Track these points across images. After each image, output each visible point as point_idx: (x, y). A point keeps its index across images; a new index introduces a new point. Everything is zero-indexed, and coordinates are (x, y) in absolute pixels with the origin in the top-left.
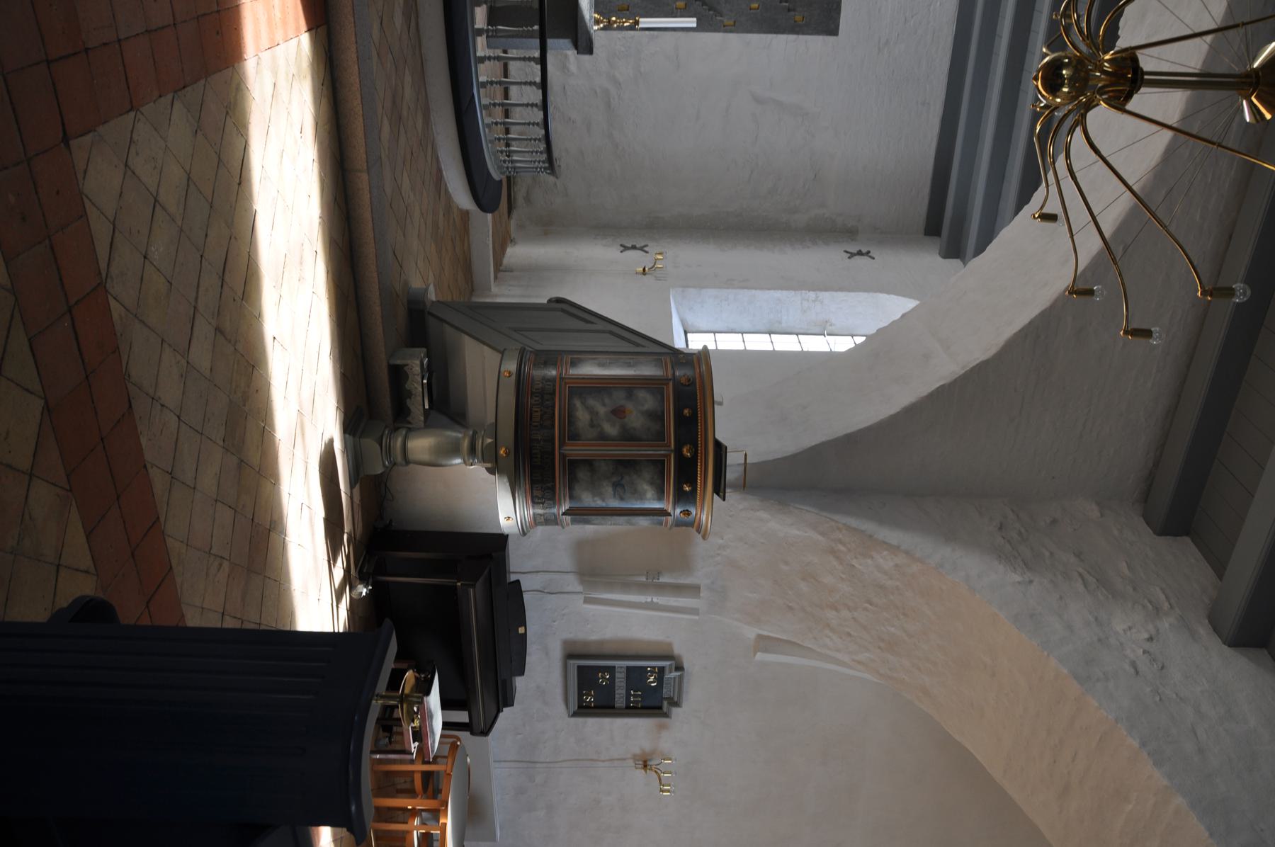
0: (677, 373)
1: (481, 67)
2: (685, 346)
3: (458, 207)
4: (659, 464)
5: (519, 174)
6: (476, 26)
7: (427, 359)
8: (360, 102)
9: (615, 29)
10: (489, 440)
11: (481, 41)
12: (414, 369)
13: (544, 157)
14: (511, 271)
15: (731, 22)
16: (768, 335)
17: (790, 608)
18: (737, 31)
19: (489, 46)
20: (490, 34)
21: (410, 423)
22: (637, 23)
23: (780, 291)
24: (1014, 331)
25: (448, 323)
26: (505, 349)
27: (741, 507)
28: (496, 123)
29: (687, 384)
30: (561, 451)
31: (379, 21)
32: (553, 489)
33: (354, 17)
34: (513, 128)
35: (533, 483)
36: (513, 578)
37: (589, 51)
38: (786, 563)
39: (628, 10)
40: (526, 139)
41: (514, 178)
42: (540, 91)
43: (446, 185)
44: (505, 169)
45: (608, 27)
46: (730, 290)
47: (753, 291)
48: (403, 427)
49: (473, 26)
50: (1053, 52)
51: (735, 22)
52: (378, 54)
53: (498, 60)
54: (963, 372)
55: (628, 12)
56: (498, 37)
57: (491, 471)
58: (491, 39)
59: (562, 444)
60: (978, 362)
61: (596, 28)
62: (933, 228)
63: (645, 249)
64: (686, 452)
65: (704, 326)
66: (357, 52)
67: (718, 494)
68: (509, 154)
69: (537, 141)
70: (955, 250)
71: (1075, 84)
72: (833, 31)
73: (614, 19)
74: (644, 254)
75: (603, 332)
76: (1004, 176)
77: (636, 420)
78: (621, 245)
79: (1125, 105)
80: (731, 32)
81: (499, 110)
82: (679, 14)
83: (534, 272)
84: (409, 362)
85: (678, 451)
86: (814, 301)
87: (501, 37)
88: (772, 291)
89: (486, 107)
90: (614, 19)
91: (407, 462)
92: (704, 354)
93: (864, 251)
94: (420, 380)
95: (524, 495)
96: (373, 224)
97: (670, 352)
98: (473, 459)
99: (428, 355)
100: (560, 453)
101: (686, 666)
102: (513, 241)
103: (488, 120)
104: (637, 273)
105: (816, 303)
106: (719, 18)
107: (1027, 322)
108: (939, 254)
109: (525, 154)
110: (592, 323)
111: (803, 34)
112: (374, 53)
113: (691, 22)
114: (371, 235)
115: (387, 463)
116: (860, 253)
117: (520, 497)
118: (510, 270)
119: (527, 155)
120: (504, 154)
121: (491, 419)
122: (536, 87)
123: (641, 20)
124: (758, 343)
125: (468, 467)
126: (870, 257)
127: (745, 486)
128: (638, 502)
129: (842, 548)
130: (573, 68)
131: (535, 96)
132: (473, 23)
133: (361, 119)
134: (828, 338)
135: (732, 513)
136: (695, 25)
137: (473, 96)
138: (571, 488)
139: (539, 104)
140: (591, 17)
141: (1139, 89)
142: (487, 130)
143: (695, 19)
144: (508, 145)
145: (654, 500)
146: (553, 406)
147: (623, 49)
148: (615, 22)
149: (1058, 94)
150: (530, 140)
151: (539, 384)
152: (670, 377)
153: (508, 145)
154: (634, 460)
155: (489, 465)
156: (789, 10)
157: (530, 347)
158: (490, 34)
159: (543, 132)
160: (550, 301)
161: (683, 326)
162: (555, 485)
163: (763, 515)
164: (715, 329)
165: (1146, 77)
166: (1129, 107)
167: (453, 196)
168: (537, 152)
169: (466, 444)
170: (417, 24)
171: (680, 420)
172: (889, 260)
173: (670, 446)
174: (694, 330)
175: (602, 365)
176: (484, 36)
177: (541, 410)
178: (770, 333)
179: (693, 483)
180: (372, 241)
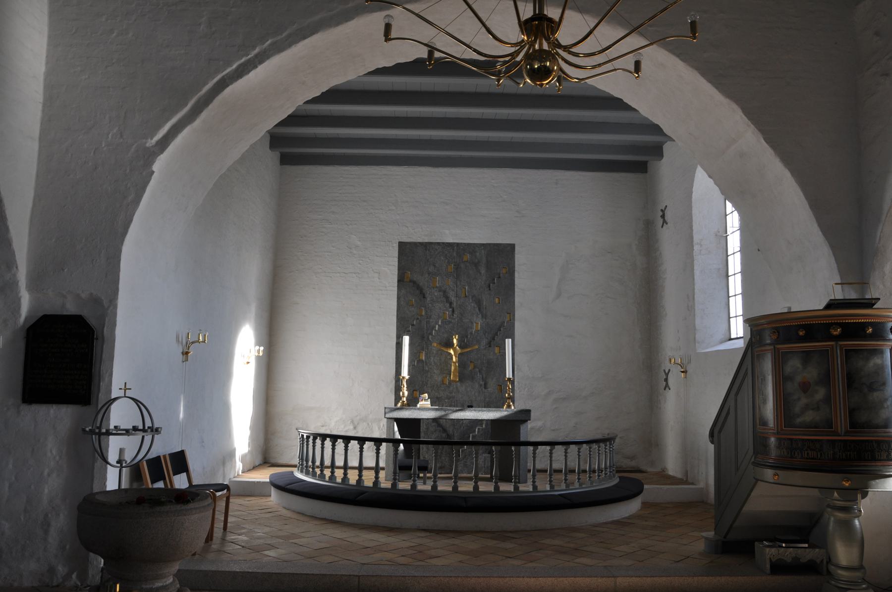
0: (768, 342)
1: (540, 488)
2: (742, 339)
3: (640, 510)
5: (615, 464)
6: (513, 490)
7: (764, 542)
8: (565, 579)
9: (514, 394)
10: (836, 494)
11: (522, 487)
12: (774, 554)
13: (602, 445)
14: (687, 472)
15: (508, 315)
16: (730, 278)
19: (525, 482)
20: (517, 481)
21: (822, 561)
22: (509, 379)
23: (695, 271)
24: (717, 92)
25: (734, 522)
26: (754, 478)
27: (881, 286)
28: (579, 479)
29: (777, 334)
30: (843, 434)
31: (509, 559)
32: (879, 443)
33: (506, 577)
34: (582, 468)
35: (874, 459)
37: (527, 412)
39: (501, 386)
40: (590, 458)
41: (617, 468)
42: (556, 446)
43: (624, 518)
44: (611, 474)
45: (512, 399)
46: (696, 308)
47: (696, 291)
48: (827, 569)
49: (512, 492)
50: (523, 77)
51: (508, 313)
52: (531, 562)
53: (535, 476)
54: (752, 125)
55: (502, 386)
56: (519, 475)
57: (865, 495)
58: (521, 481)
59: (836, 433)
60: (744, 116)
61: (513, 407)
62: (640, 167)
63: (667, 371)
64: (837, 332)
65: (725, 326)
66: (530, 577)
67: (874, 304)
68: (600, 470)
69: (591, 450)
70: (657, 151)
71: (544, 58)
72: (512, 246)
73: (507, 395)
74: (670, 372)
75: (736, 401)
76: (603, 123)
77: (811, 373)
78: (665, 389)
79: (557, 22)
80: (514, 315)
81: (569, 477)
82: (503, 351)
83: (688, 453)
84: (768, 557)
86: (701, 245)
87: (519, 473)
88: (695, 277)
89: (567, 486)
90: (507, 395)
91: (860, 568)
92: (751, 322)
93: (661, 213)
94: (783, 549)
95: (887, 467)
96: (656, 576)
97: (750, 348)
98: (854, 509)
99: (761, 541)
100: (844, 436)
102: (664, 470)
103: (577, 485)
104: (686, 377)
105: (702, 244)
106: (505, 324)
107: (710, 84)
108: (660, 160)
109: (600, 459)
110: (729, 410)
111: (514, 267)
112: (531, 565)
113: (508, 342)
114: (664, 579)
115: (864, 586)
116: (663, 216)
117: (888, 470)
118: (686, 473)
119: (601, 457)
120: (600, 474)
121: (816, 492)
122: (553, 449)
123: (507, 377)
124: (736, 284)
125: (863, 514)
126: (665, 209)
127: (863, 283)
128: (886, 370)
130: (539, 424)
131: (559, 450)
132: (510, 492)
133: (578, 579)
134: (728, 233)
135: (888, 294)
136: (510, 340)
137: (559, 495)
138: (878, 427)
139: (565, 448)
140: (506, 411)
141: (546, 15)
142: (583, 486)
143: (506, 340)
144: (594, 471)
145: (883, 357)
146: (803, 440)
147: (526, 389)
148: (509, 394)
149: (551, 69)
150: (590, 455)
151: (783, 452)
152: (772, 347)
153: (594, 471)
154: (847, 375)
155: (859, 496)
157: (752, 457)
158: (517, 481)
159: (584, 445)
160: (712, 442)
161: (725, 341)
162: (875, 440)
164: (727, 317)
165: (537, 13)
166: (557, 19)
167: (631, 514)
168: (599, 450)
169: (841, 515)
170: (511, 532)
171: (809, 338)
172: (667, 196)
173: (832, 345)
174: (728, 333)
175: (765, 401)
176: (519, 485)
177: (807, 450)
178: (727, 276)
179: (864, 326)
180: (669, 578)
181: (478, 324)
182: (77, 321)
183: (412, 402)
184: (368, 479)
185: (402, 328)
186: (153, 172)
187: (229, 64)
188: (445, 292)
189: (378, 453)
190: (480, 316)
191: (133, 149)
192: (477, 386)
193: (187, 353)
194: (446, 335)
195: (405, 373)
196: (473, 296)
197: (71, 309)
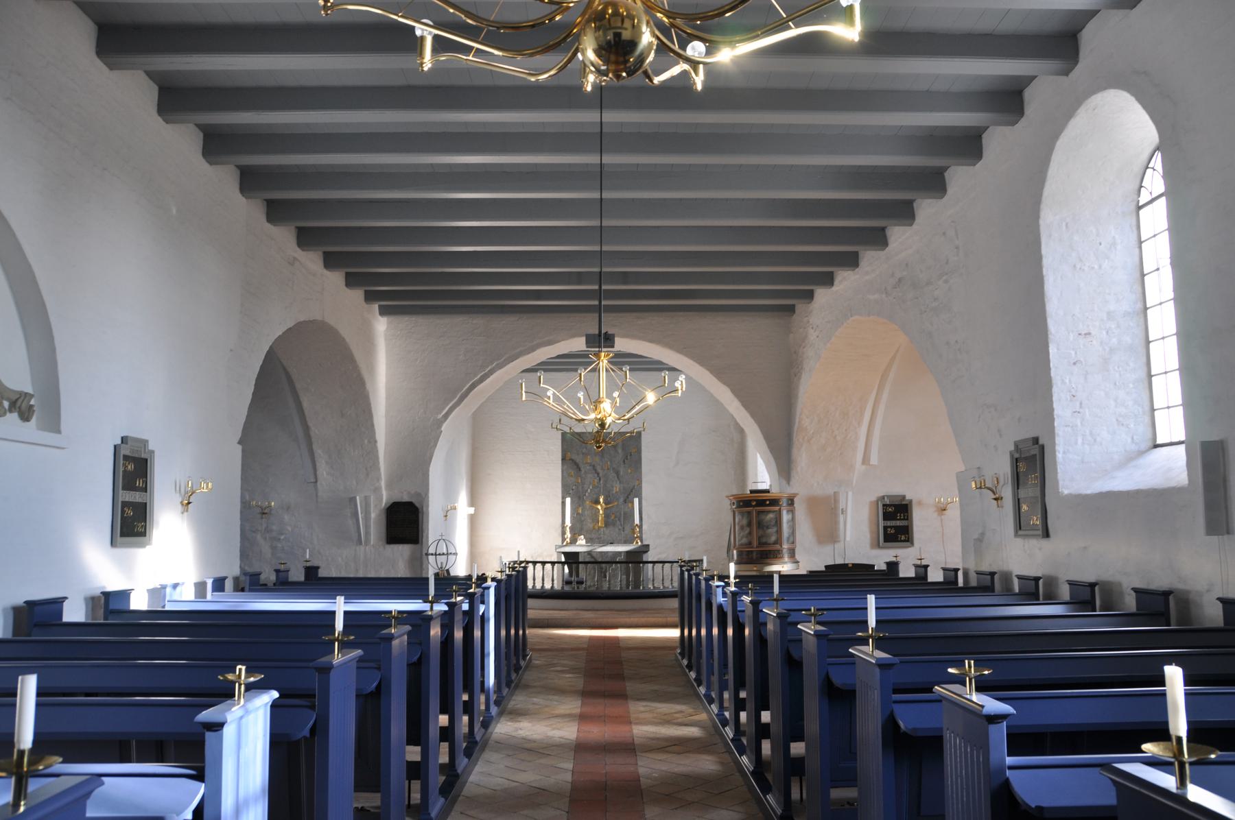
2: (1183, 447)
4: (759, 513)
17: (841, 454)
18: (641, 478)
35: (767, 558)
36: (824, 569)
38: (820, 458)
59: (752, 547)
85: (754, 506)
101: (882, 495)
113: (636, 500)
123: (636, 523)
129: (806, 438)
156: (631, 455)
163: (799, 469)
181: (617, 487)
182: (410, 504)
183: (573, 541)
184: (548, 586)
185: (566, 491)
186: (442, 431)
187: (475, 376)
188: (594, 466)
189: (553, 568)
190: (618, 482)
191: (432, 420)
192: (617, 530)
193: (446, 516)
194: (595, 496)
195: (568, 523)
196: (613, 469)
197: (406, 499)
